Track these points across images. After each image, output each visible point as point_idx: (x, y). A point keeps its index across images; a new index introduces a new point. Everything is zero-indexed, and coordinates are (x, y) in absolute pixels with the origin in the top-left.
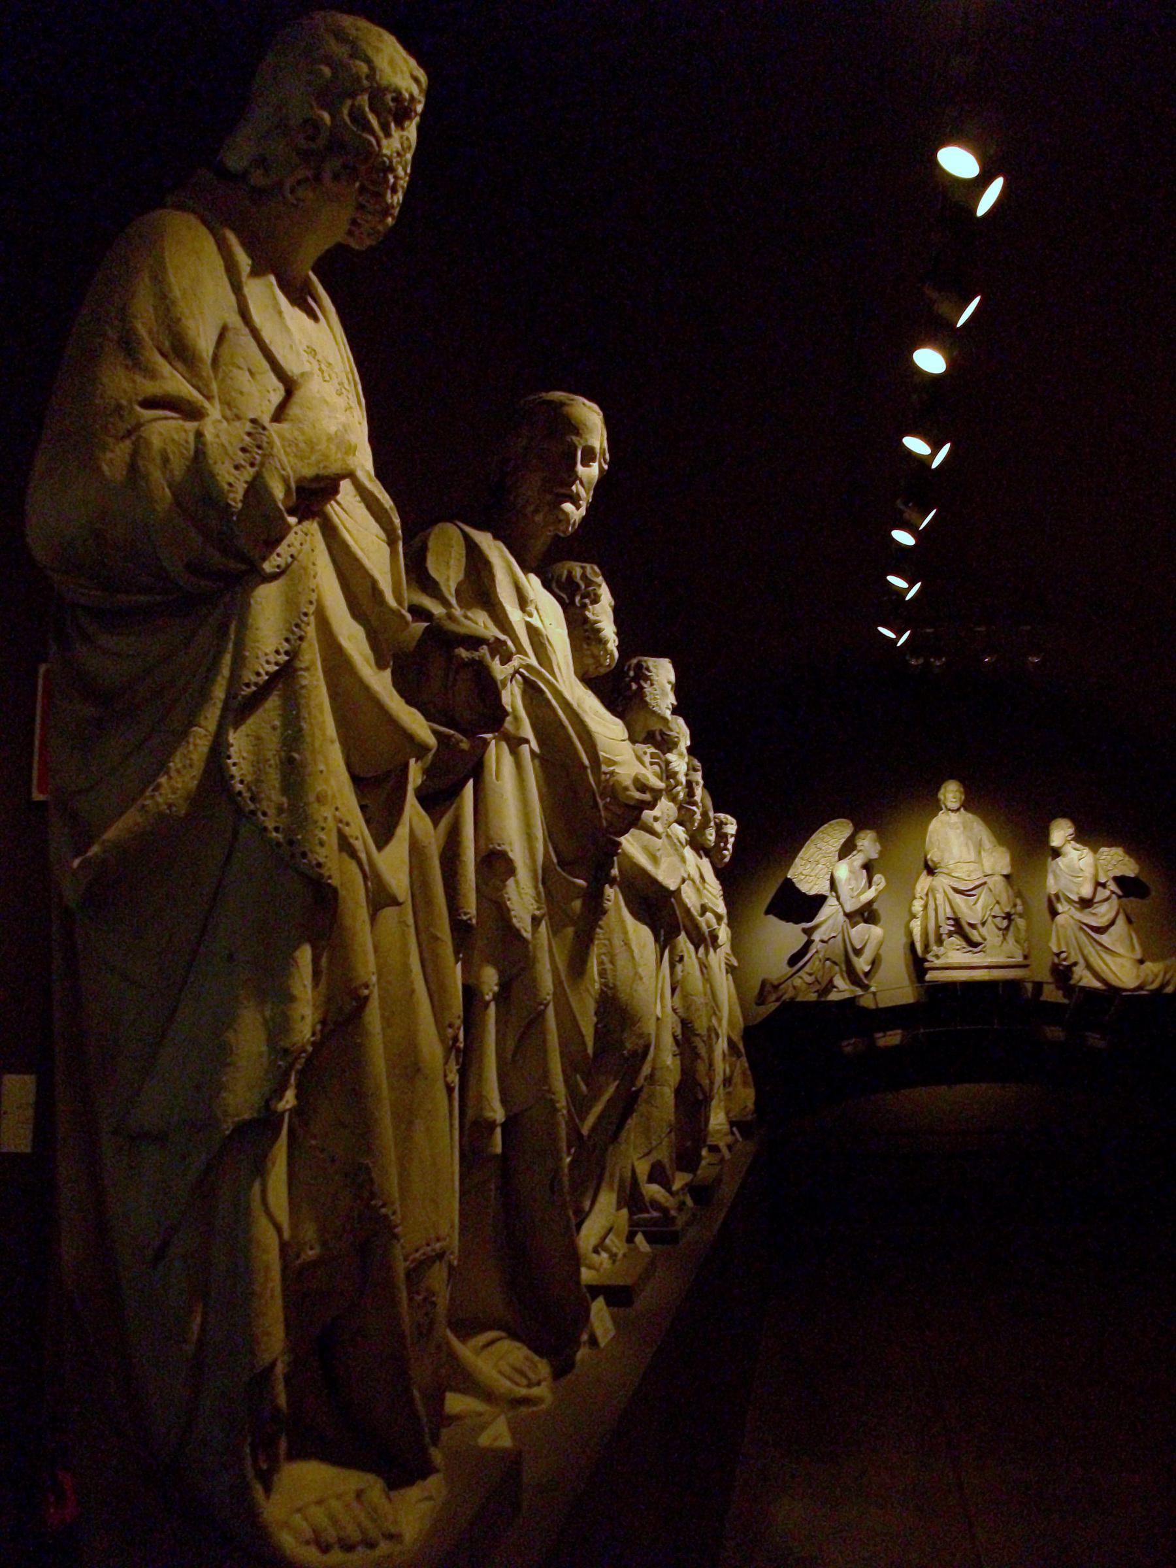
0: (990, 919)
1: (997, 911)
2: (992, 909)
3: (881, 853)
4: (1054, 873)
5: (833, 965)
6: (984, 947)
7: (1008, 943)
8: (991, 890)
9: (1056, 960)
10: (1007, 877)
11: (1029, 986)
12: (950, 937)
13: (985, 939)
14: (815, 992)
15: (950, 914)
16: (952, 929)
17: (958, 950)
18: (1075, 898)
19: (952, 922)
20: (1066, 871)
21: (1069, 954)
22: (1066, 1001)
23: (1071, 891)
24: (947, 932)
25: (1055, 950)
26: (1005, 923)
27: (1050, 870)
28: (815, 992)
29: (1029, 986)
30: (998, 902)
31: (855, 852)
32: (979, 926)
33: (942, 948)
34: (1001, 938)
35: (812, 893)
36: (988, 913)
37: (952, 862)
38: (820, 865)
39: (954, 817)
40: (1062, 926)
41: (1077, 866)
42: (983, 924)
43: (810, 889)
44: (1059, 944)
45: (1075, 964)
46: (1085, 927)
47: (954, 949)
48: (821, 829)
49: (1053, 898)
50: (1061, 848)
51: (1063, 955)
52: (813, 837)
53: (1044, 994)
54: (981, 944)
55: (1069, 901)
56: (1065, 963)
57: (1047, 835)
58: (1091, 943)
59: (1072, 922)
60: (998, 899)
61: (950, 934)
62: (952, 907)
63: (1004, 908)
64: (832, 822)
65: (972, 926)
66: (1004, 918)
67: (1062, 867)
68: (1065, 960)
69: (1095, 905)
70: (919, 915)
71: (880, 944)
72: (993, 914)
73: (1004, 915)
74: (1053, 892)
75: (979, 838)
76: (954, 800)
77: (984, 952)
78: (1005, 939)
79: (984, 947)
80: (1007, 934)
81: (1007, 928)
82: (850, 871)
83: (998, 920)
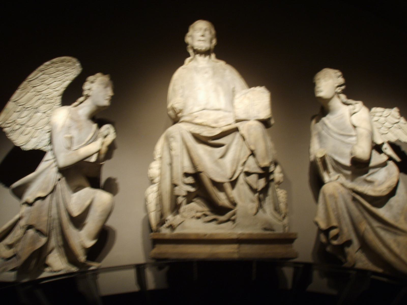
0: (242, 177)
1: (252, 165)
2: (244, 163)
3: (113, 99)
4: (320, 136)
5: (37, 234)
6: (234, 214)
7: (264, 212)
8: (244, 139)
9: (323, 239)
10: (265, 123)
11: (288, 272)
12: (189, 202)
13: (235, 204)
14: (13, 270)
15: (190, 170)
16: (192, 189)
17: (199, 218)
18: (347, 162)
19: (190, 180)
20: (335, 129)
21: (341, 230)
22: (334, 292)
23: (342, 155)
24: (184, 194)
25: (323, 226)
26: (262, 183)
27: (314, 133)
28: (13, 270)
29: (288, 272)
30: (253, 154)
31: (81, 99)
32: (228, 186)
33: (178, 217)
34: (256, 205)
35: (29, 147)
36: (240, 168)
37: (196, 109)
38: (39, 114)
39: (202, 61)
40: (332, 196)
41: (348, 123)
42: (233, 183)
43: (28, 142)
44: (328, 217)
45: (349, 243)
46: (358, 197)
47: (193, 217)
48: (42, 67)
49: (319, 164)
50: (328, 100)
51: (333, 232)
52: (31, 76)
53: (58, 258)
54: (229, 210)
55: (339, 167)
56: (335, 242)
57: (312, 86)
58: (365, 218)
59: (342, 189)
60: (253, 148)
61: (190, 198)
62: (191, 159)
63: (260, 160)
64: (54, 60)
65: (219, 186)
66: (260, 176)
67: (330, 125)
68: (336, 237)
69: (371, 171)
70: (157, 180)
71: (108, 214)
72: (246, 169)
73: (260, 171)
74: (320, 155)
75: (232, 87)
76: (203, 38)
77: (234, 221)
78: (260, 206)
79: (234, 214)
80: (264, 199)
81: (264, 191)
82: (72, 119)
83: (252, 179)
